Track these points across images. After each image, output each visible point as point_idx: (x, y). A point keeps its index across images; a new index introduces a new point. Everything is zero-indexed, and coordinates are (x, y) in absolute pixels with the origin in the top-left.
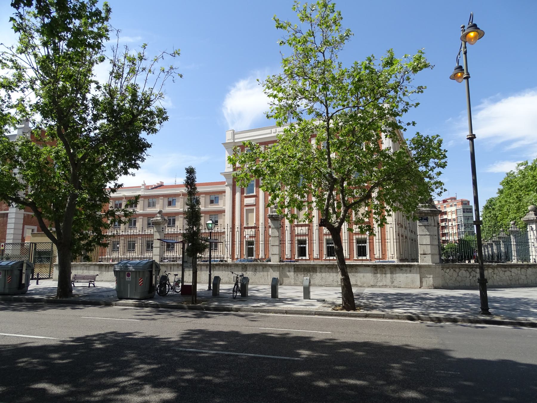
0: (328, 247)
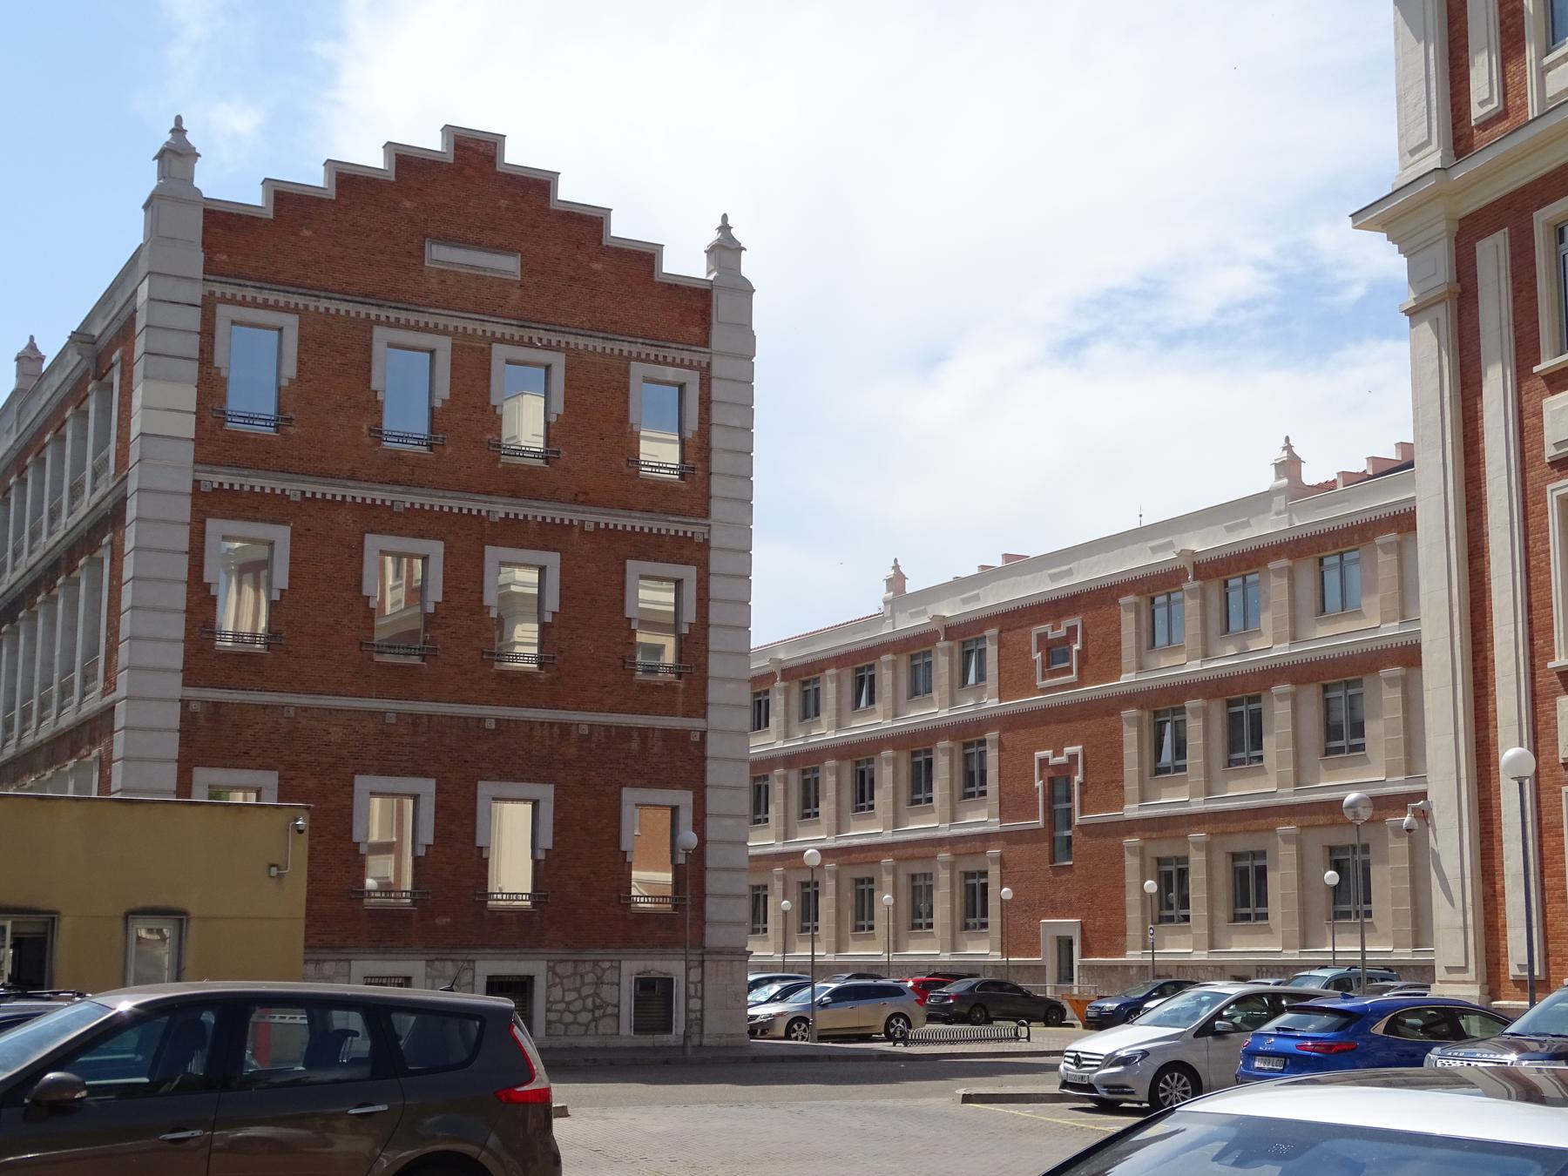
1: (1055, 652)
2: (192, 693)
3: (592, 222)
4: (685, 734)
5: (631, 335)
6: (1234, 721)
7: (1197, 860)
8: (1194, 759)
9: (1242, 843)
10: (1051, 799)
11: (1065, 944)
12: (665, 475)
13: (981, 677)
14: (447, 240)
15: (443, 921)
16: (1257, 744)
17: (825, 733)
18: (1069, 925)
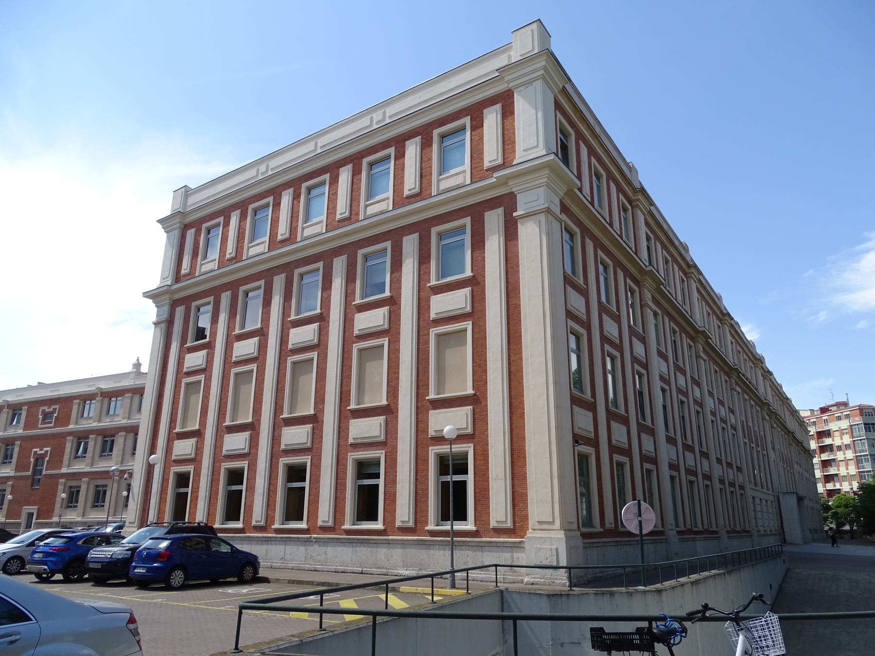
0: (290, 489)
1: (46, 416)
6: (105, 443)
7: (84, 487)
8: (89, 454)
9: (100, 482)
10: (36, 465)
11: (30, 515)
13: (18, 422)
16: (111, 450)
18: (34, 509)
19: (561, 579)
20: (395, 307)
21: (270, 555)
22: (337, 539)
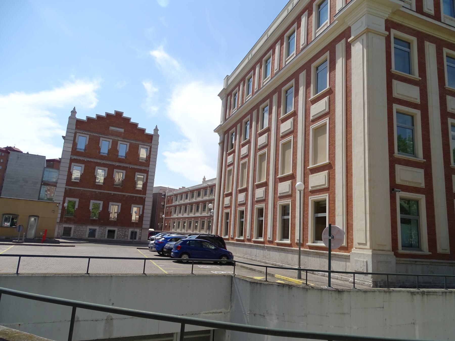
2: (67, 187)
3: (136, 125)
4: (142, 197)
5: (140, 141)
12: (144, 161)
14: (113, 126)
15: (102, 221)
17: (194, 200)
19: (368, 281)
20: (296, 117)
21: (238, 253)
22: (317, 252)
